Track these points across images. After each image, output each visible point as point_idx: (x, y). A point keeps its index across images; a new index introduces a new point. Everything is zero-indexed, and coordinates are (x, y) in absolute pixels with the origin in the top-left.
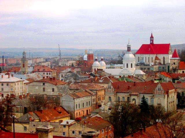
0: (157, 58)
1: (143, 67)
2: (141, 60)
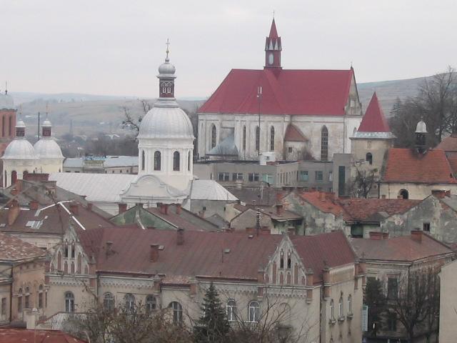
1: (230, 169)
2: (221, 139)
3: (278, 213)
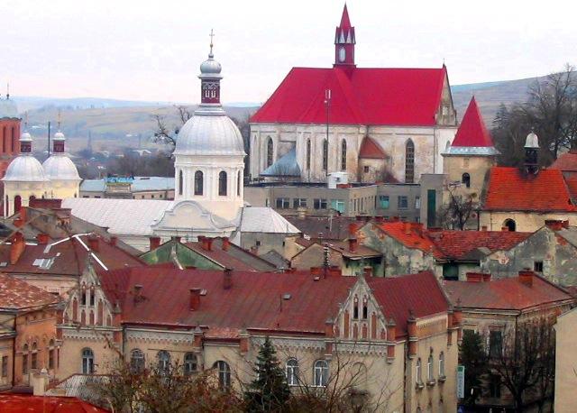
0: (369, 148)
1: (290, 193)
2: (279, 156)
3: (351, 249)
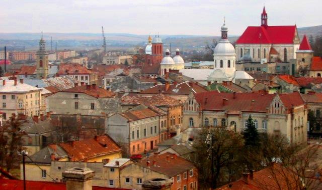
0: (273, 51)
1: (249, 66)
2: (245, 54)
3: (271, 84)
